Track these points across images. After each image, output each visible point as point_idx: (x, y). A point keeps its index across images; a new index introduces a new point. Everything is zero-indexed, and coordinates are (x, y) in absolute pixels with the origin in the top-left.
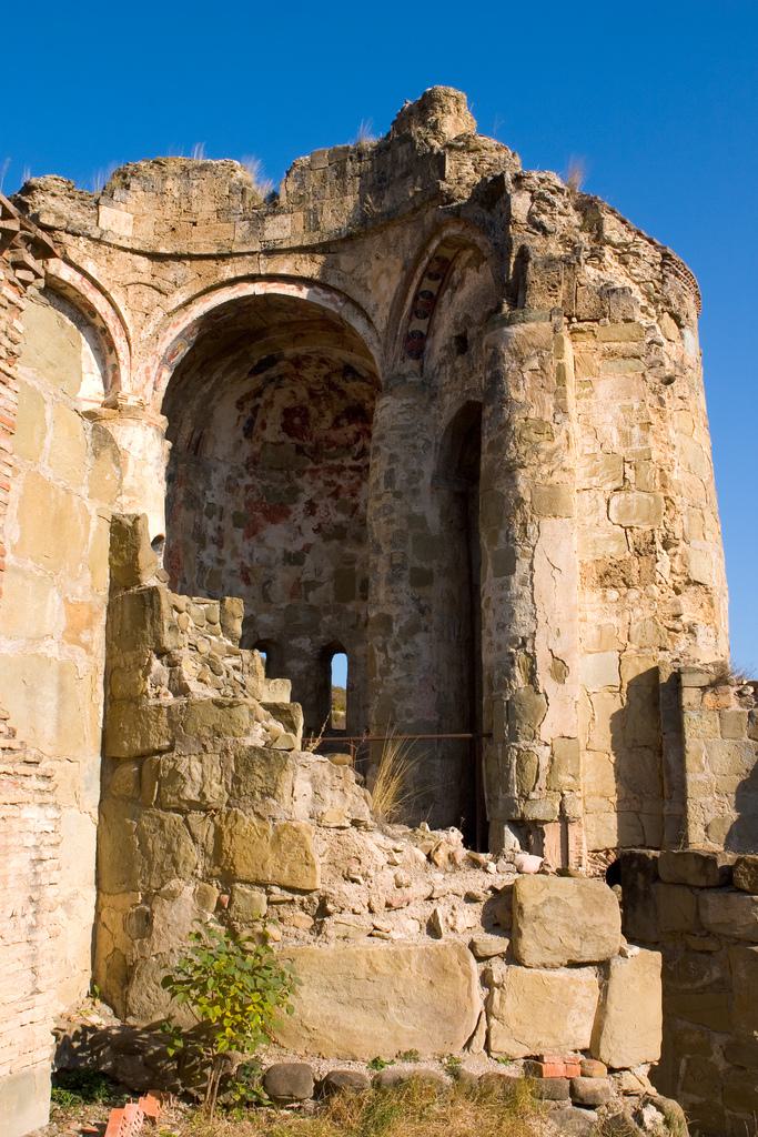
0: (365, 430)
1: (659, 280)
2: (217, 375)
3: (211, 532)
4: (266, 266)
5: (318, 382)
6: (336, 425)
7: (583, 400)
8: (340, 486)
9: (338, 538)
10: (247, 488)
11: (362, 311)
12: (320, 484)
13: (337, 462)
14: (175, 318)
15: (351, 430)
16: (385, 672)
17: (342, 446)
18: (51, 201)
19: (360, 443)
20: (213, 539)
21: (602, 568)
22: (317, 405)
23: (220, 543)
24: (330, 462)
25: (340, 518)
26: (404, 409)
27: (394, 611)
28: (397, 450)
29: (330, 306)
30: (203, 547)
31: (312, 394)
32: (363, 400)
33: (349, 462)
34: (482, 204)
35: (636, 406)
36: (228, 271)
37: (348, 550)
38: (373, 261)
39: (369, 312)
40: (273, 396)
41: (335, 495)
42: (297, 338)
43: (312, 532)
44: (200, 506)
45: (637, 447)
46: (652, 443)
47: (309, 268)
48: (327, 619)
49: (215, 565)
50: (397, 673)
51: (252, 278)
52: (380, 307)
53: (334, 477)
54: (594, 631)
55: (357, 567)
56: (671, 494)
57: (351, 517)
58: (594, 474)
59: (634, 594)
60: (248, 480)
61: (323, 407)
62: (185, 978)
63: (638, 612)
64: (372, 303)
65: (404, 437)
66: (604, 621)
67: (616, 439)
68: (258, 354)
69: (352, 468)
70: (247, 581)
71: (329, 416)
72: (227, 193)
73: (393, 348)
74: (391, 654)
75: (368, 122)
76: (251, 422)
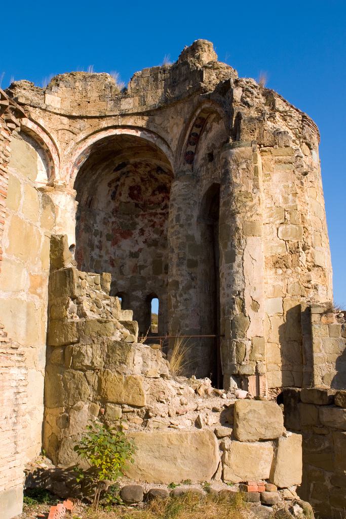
0: (167, 196)
1: (301, 128)
2: (99, 171)
3: (96, 243)
4: (121, 122)
5: (145, 174)
6: (153, 194)
7: (266, 183)
8: (155, 222)
9: (154, 246)
10: (113, 223)
11: (165, 142)
12: (146, 221)
13: (154, 211)
14: (80, 145)
15: (160, 196)
16: (176, 307)
17: (156, 204)
18: (23, 92)
19: (164, 202)
20: (97, 246)
21: (275, 259)
22: (144, 185)
23: (100, 248)
24: (151, 211)
25: (155, 236)
26: (184, 187)
27: (180, 279)
28: (181, 206)
29: (151, 140)
30: (93, 250)
31: (142, 180)
32: (166, 183)
33: (159, 211)
34: (220, 93)
35: (290, 185)
36: (104, 124)
37: (159, 251)
38: (170, 119)
39: (169, 142)
40: (125, 181)
41: (153, 226)
42: (135, 154)
43: (142, 243)
44: (91, 231)
45: (291, 204)
46: (297, 202)
47: (141, 123)
48: (149, 282)
49: (98, 258)
50: (181, 307)
51: (115, 127)
52: (174, 140)
53: (153, 218)
54: (271, 288)
55: (163, 259)
56: (306, 225)
57: (160, 236)
58: (271, 216)
59: (289, 271)
60: (113, 219)
61: (147, 186)
62: (84, 447)
63: (291, 279)
64: (170, 138)
65: (184, 199)
66: (276, 284)
67: (281, 200)
68: (118, 162)
69: (160, 214)
70: (113, 265)
71: (150, 190)
72: (104, 88)
73: (180, 159)
74: (178, 299)
75: (168, 56)
76: (114, 193)
